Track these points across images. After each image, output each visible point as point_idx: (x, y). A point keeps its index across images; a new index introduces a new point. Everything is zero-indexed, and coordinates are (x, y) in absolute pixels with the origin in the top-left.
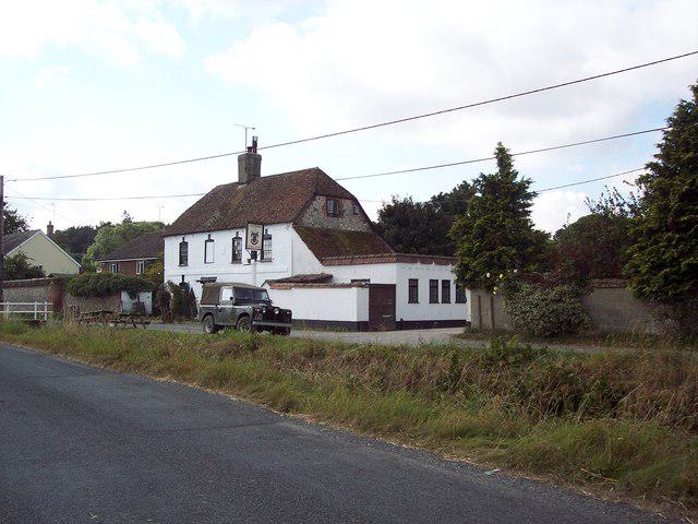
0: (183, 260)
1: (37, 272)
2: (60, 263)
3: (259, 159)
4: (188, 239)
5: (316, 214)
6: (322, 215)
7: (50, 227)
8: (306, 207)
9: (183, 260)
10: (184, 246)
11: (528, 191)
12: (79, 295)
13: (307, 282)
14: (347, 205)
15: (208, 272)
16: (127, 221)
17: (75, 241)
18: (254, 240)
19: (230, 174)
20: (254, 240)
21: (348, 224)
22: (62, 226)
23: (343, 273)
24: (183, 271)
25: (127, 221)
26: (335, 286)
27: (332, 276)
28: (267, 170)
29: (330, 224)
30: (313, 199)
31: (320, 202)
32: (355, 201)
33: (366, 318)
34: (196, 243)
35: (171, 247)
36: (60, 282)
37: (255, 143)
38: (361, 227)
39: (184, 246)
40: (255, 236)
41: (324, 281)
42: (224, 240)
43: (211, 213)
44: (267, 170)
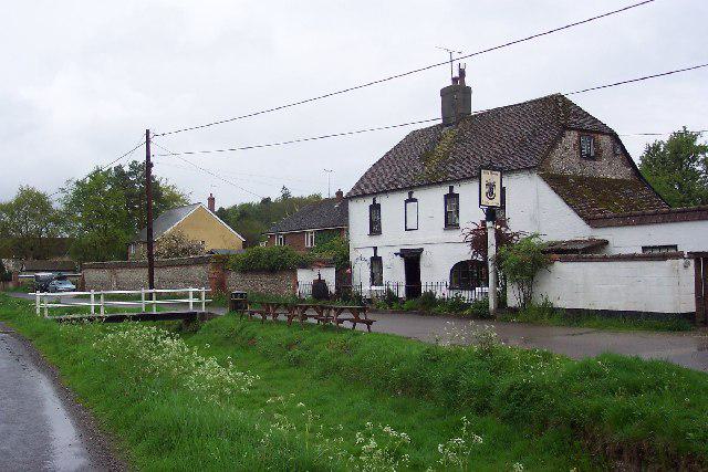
0: (375, 228)
1: (553, 311)
2: (227, 240)
3: (468, 91)
4: (383, 201)
5: (565, 157)
6: (575, 159)
7: (212, 200)
8: (553, 146)
9: (375, 228)
10: (375, 208)
11: (697, 144)
12: (244, 271)
13: (585, 251)
14: (605, 140)
15: (412, 241)
16: (286, 196)
17: (240, 217)
18: (491, 194)
19: (430, 114)
20: (491, 194)
21: (608, 170)
22: (225, 202)
23: (626, 239)
24: (375, 241)
25: (286, 196)
26: (605, 259)
27: (607, 243)
28: (479, 104)
29: (589, 169)
30: (562, 135)
31: (571, 138)
32: (614, 137)
33: (688, 305)
34: (392, 206)
35: (359, 213)
36: (221, 261)
37: (462, 73)
38: (624, 173)
39: (375, 208)
40: (491, 186)
41: (592, 251)
42: (431, 201)
43: (379, 182)
44: (479, 104)
